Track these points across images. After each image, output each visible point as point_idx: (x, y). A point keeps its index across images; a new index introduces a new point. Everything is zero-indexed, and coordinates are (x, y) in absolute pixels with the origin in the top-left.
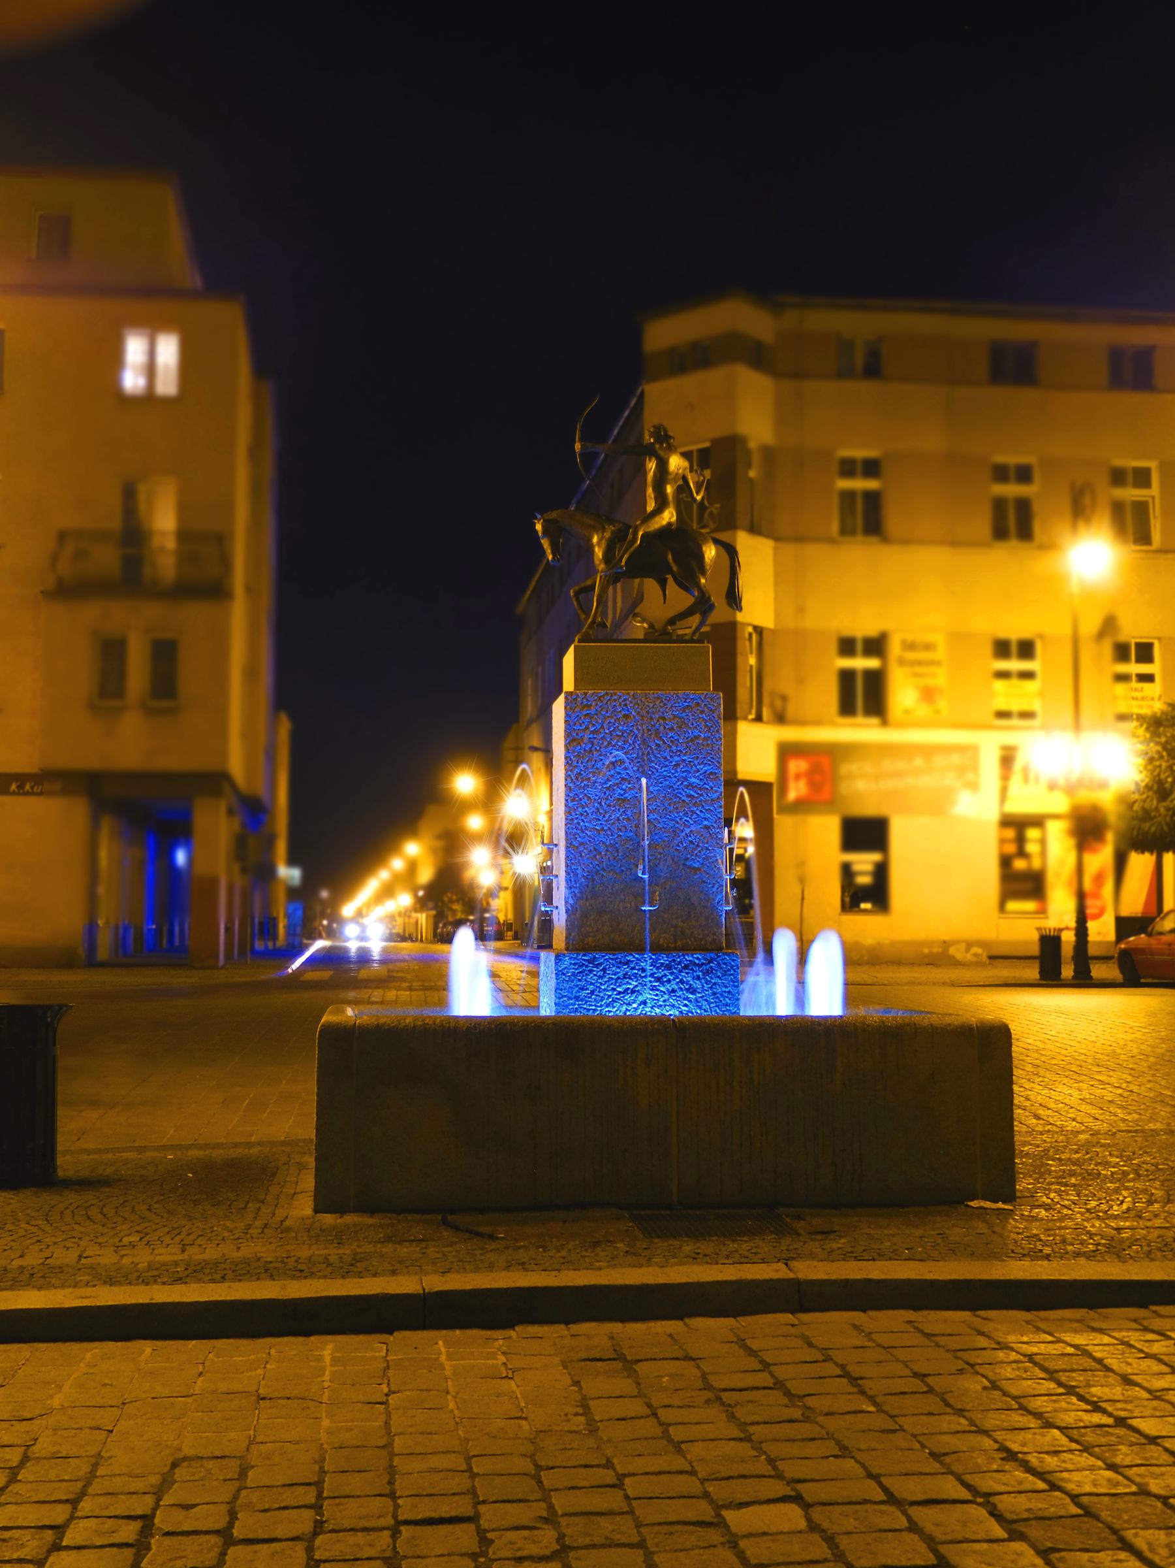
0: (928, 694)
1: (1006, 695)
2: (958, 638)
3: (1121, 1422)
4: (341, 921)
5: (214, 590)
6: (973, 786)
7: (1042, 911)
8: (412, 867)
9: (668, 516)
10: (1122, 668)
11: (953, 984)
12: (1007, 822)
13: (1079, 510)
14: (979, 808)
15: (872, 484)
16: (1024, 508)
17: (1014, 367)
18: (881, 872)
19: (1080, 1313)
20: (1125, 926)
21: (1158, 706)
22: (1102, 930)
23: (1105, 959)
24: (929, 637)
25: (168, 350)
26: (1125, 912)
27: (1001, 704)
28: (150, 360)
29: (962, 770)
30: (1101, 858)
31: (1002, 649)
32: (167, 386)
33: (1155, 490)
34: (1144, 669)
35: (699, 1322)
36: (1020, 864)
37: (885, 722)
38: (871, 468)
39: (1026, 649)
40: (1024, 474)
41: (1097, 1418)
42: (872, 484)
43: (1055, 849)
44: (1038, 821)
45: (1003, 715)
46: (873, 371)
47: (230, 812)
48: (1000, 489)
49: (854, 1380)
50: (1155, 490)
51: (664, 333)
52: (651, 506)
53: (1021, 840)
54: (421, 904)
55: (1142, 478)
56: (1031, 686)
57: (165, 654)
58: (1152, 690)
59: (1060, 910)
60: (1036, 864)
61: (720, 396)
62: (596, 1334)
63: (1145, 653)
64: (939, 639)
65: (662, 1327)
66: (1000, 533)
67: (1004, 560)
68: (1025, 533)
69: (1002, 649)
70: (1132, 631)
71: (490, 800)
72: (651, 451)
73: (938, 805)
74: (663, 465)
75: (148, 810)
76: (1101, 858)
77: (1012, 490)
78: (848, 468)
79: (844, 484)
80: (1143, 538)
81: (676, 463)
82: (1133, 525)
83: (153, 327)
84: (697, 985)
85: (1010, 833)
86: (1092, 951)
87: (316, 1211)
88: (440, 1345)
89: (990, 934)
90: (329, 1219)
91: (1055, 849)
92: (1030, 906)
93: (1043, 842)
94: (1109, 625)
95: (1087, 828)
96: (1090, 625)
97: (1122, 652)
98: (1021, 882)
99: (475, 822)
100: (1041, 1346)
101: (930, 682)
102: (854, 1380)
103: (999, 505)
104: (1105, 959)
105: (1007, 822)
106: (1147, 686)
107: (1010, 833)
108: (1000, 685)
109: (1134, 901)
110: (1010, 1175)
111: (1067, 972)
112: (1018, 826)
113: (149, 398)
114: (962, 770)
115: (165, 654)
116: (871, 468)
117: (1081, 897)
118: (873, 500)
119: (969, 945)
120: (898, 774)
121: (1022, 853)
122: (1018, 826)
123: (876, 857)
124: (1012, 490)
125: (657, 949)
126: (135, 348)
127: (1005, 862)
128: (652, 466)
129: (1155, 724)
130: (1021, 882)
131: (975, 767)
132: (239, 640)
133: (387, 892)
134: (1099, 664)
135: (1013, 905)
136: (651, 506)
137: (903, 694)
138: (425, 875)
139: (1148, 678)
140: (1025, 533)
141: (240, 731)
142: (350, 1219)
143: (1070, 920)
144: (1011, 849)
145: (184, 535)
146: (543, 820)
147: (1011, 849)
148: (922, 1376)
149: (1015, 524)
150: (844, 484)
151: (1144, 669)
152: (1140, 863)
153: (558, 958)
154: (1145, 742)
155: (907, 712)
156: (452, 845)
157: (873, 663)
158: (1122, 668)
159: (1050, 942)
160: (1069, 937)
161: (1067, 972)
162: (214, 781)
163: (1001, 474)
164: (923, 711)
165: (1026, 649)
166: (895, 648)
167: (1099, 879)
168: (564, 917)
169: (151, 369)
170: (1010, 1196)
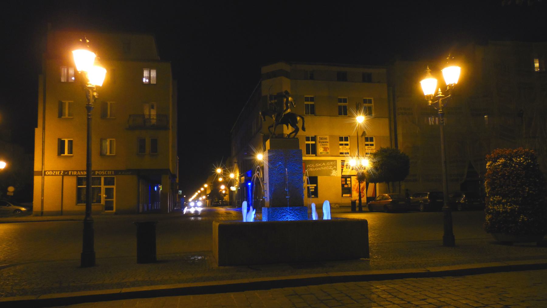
0: (325, 149)
1: (342, 149)
2: (331, 137)
3: (409, 302)
4: (189, 202)
5: (166, 128)
6: (336, 169)
7: (351, 196)
8: (205, 189)
9: (289, 111)
10: (367, 143)
11: (337, 213)
12: (343, 177)
13: (358, 108)
14: (337, 174)
15: (312, 103)
16: (345, 107)
17: (342, 77)
18: (316, 188)
19: (390, 281)
20: (368, 199)
21: (374, 151)
22: (364, 200)
23: (365, 206)
24: (326, 137)
25: (154, 74)
26: (368, 196)
27: (341, 151)
28: (149, 76)
29: (333, 166)
30: (363, 184)
31: (341, 139)
32: (153, 82)
33: (373, 104)
34: (371, 143)
35: (310, 286)
36: (346, 186)
37: (316, 156)
38: (312, 99)
39: (346, 139)
40: (345, 101)
41: (403, 302)
42: (312, 103)
43: (354, 182)
44: (350, 177)
45: (341, 153)
46: (312, 78)
47: (169, 178)
48: (340, 104)
49: (350, 297)
50: (373, 104)
51: (265, 69)
52: (285, 109)
53: (346, 181)
54: (207, 198)
55: (370, 101)
56: (348, 147)
57: (154, 143)
58: (373, 147)
59: (355, 195)
60: (349, 186)
61: (278, 83)
62: (290, 290)
63: (371, 140)
64: (328, 137)
65: (302, 288)
66: (340, 114)
67: (340, 119)
68: (346, 114)
69: (341, 139)
70: (368, 135)
71: (225, 174)
72: (285, 97)
73: (328, 173)
74: (287, 99)
75: (149, 178)
76: (363, 184)
77: (342, 104)
78: (307, 99)
79: (306, 103)
80: (370, 114)
81: (290, 99)
82: (368, 112)
83: (150, 68)
84: (298, 213)
85: (344, 179)
86: (362, 205)
87: (219, 266)
88: (257, 293)
89: (340, 201)
90: (222, 267)
91: (354, 182)
92: (349, 195)
93: (351, 181)
94: (364, 133)
95: (361, 178)
96: (360, 134)
97: (367, 139)
98: (347, 190)
99: (220, 179)
100: (384, 287)
101: (326, 146)
102: (350, 297)
103: (340, 107)
104: (365, 206)
105: (343, 177)
106: (347, 146)
107: (344, 179)
108: (341, 147)
109: (370, 193)
110: (368, 252)
111: (357, 209)
112: (345, 178)
113: (149, 84)
114: (333, 166)
115: (154, 143)
116: (312, 99)
117: (360, 193)
118: (312, 106)
119: (335, 204)
120: (320, 167)
121: (346, 184)
122: (345, 178)
123: (315, 185)
124: (342, 104)
125: (290, 206)
126: (146, 73)
127: (343, 185)
128: (285, 100)
129: (375, 155)
130: (347, 190)
131: (336, 165)
132: (170, 140)
133: (199, 195)
134: (362, 142)
135: (344, 195)
136: (285, 109)
137: (320, 150)
138: (209, 192)
139: (372, 145)
140: (346, 114)
141: (171, 161)
142: (227, 267)
143: (358, 198)
144: (344, 183)
145: (158, 115)
146: (237, 178)
147: (344, 183)
148: (364, 295)
149: (344, 112)
150: (306, 103)
151: (371, 143)
152: (371, 185)
153: (268, 209)
154: (373, 159)
155: (321, 153)
156: (215, 186)
157: (314, 142)
158: (367, 143)
159: (353, 203)
160: (357, 202)
161: (357, 209)
162: (166, 171)
163: (340, 101)
164: (324, 153)
165: (346, 139)
166: (318, 139)
167: (363, 189)
168: (268, 200)
169: (149, 78)
170: (368, 257)
